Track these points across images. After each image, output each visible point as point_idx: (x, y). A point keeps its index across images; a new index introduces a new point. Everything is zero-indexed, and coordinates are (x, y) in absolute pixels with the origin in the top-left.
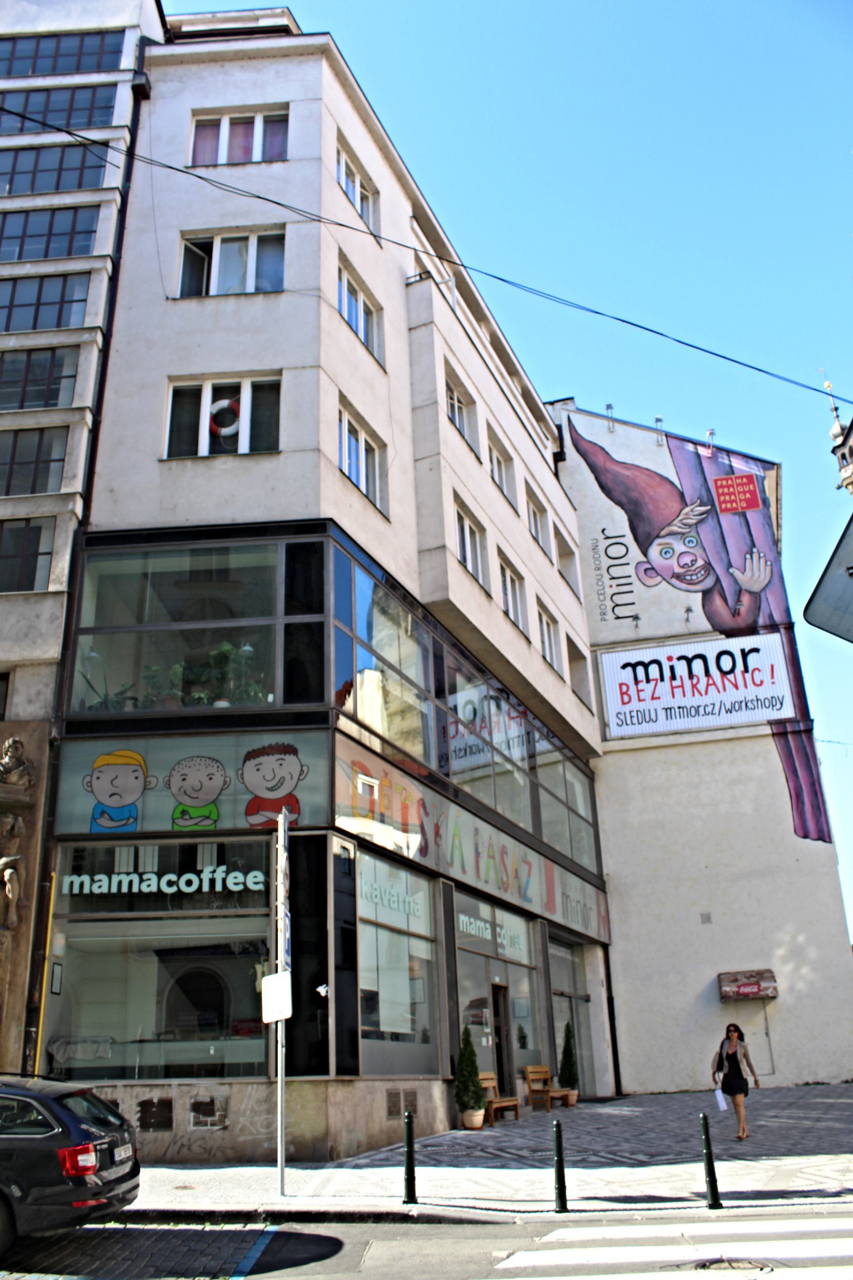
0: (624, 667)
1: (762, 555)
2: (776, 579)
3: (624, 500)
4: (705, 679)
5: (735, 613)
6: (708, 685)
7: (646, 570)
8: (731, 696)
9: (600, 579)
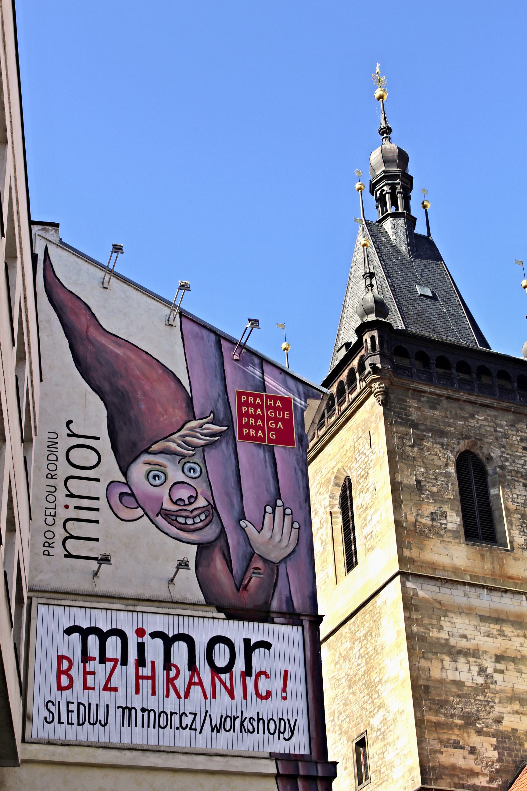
0: (70, 631)
1: (288, 511)
2: (303, 550)
3: (106, 387)
4: (188, 674)
5: (241, 586)
6: (191, 683)
7: (122, 495)
8: (222, 706)
9: (52, 492)
